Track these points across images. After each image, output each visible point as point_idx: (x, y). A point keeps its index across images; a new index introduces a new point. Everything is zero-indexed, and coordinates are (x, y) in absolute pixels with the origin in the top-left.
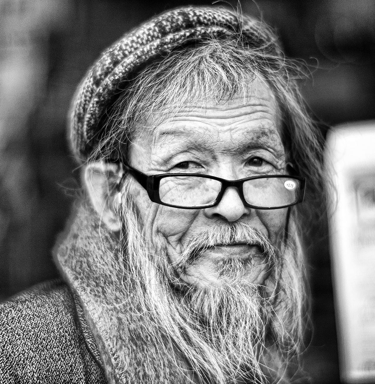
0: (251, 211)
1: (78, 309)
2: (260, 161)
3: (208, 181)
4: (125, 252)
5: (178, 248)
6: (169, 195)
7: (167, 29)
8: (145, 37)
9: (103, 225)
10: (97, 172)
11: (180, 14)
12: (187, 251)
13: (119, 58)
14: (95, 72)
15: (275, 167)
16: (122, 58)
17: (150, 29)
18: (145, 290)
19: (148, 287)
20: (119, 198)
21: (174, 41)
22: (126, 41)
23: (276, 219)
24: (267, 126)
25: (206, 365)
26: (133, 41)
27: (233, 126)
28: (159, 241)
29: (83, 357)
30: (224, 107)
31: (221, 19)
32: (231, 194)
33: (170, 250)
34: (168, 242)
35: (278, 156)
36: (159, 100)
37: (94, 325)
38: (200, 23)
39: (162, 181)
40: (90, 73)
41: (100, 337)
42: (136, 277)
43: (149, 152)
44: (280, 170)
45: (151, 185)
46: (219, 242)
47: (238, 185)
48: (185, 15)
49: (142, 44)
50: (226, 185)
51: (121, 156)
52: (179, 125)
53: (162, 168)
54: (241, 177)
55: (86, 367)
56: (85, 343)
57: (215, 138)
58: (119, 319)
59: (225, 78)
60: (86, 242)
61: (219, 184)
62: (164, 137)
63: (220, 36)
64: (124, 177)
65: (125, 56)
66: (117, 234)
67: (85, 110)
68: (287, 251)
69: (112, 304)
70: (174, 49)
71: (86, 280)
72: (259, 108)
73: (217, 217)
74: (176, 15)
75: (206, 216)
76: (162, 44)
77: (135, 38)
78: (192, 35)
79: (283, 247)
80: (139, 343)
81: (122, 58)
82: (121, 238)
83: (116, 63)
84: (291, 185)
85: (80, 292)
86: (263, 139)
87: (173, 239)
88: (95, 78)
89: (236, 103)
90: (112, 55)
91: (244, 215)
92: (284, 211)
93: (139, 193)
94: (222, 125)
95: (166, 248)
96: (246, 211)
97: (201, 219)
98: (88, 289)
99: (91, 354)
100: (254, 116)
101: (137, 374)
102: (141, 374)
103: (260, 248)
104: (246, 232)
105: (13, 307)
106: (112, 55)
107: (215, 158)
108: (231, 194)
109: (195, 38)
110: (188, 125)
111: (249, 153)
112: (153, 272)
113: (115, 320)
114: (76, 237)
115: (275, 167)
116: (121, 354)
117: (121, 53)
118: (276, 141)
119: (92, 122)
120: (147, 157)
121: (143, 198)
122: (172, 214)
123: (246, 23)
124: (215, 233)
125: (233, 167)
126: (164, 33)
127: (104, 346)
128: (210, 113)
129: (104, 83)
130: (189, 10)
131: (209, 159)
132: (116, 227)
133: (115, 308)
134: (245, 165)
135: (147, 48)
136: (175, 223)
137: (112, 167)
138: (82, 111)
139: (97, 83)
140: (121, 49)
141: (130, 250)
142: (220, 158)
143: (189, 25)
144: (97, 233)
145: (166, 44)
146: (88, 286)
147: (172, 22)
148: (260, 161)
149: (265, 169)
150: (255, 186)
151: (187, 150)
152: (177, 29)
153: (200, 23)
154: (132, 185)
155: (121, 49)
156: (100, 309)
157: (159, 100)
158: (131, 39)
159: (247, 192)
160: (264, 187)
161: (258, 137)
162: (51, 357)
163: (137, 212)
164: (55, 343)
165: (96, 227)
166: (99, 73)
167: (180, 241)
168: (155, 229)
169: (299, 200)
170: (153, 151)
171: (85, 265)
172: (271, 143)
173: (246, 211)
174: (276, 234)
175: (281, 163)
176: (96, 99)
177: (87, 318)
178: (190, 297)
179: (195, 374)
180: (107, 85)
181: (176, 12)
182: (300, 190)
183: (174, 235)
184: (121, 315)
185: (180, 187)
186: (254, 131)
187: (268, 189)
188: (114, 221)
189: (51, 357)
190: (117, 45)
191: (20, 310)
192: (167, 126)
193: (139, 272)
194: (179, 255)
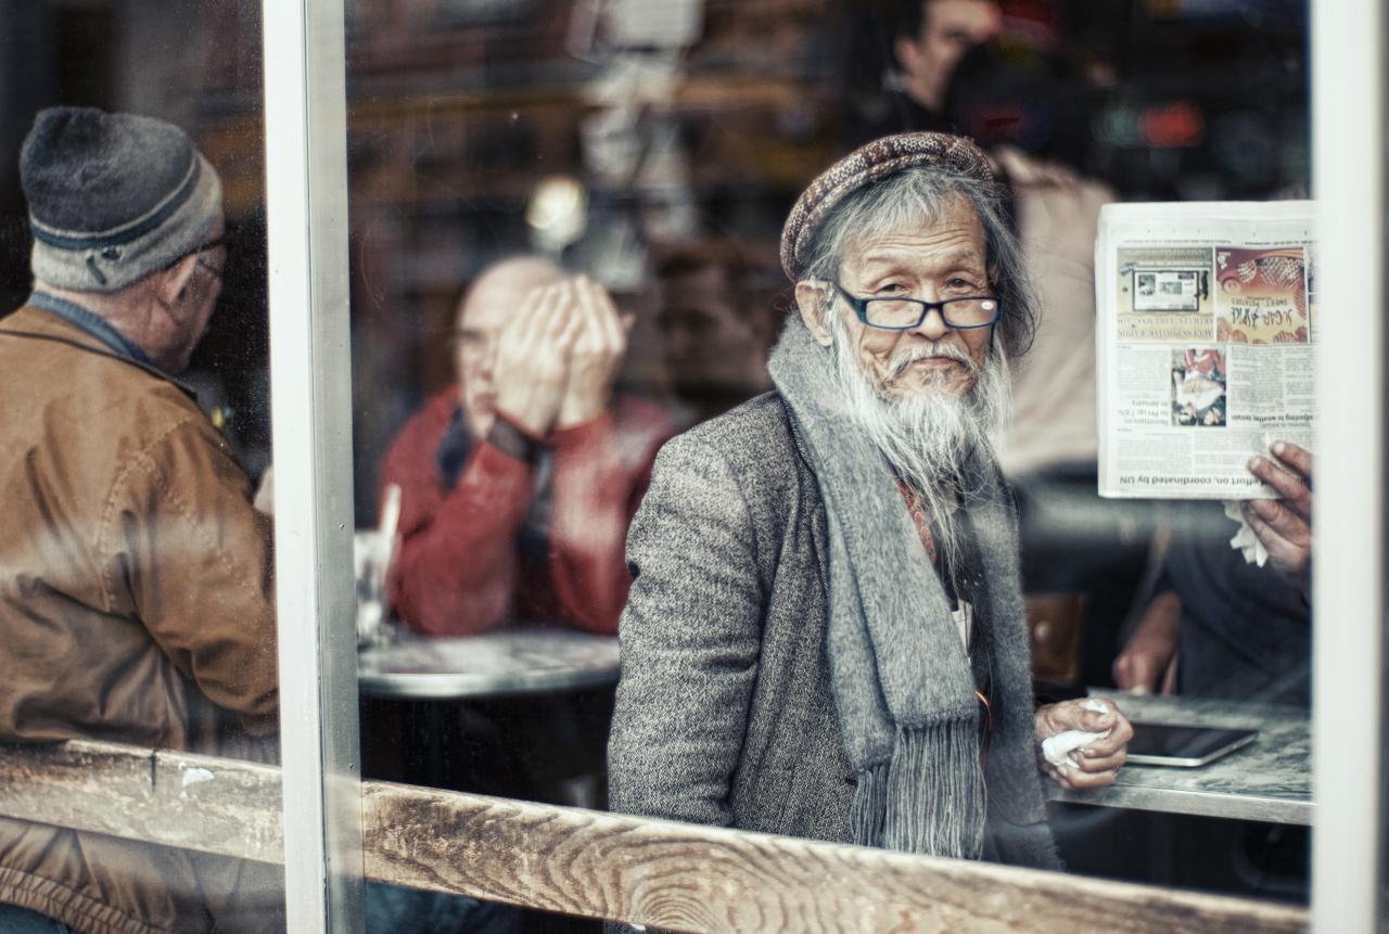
0: (950, 330)
1: (792, 421)
2: (961, 283)
3: (911, 304)
4: (836, 366)
5: (885, 363)
6: (875, 316)
7: (873, 159)
8: (853, 168)
9: (815, 340)
10: (808, 289)
11: (885, 144)
12: (894, 365)
13: (828, 187)
14: (806, 199)
15: (975, 287)
16: (832, 188)
17: (856, 161)
18: (854, 402)
19: (856, 400)
20: (831, 315)
21: (879, 171)
22: (835, 171)
23: (977, 337)
24: (966, 249)
25: (912, 472)
26: (841, 172)
27: (934, 252)
28: (868, 357)
29: (796, 464)
30: (925, 235)
31: (924, 146)
32: (933, 316)
33: (878, 365)
34: (875, 358)
35: (979, 277)
36: (866, 229)
37: (807, 435)
38: (905, 152)
39: (869, 304)
40: (801, 200)
41: (813, 446)
42: (921, 434)
43: (858, 276)
44: (979, 289)
45: (861, 307)
46: (922, 356)
47: (939, 307)
48: (890, 145)
49: (850, 174)
50: (927, 307)
51: (832, 277)
52: (885, 252)
53: (870, 291)
54: (943, 298)
55: (799, 474)
56: (799, 452)
57: (918, 264)
58: (831, 430)
59: (926, 211)
60: (798, 357)
61: (920, 307)
62: (870, 264)
63: (924, 164)
64: (834, 296)
65: (834, 186)
66: (828, 348)
67: (797, 233)
68: (992, 370)
69: (823, 416)
70: (878, 180)
71: (799, 394)
72: (960, 233)
73: (919, 335)
74: (881, 144)
75: (910, 334)
76: (868, 176)
77: (843, 169)
78: (896, 165)
79: (987, 362)
80: (848, 451)
81: (832, 188)
82: (832, 350)
83: (826, 192)
84: (988, 305)
85: (794, 405)
86: (963, 262)
87: (880, 356)
88: (806, 205)
89: (938, 230)
90: (822, 183)
91: (945, 334)
92: (990, 327)
93: (848, 313)
94: (924, 251)
95: (873, 364)
96: (947, 330)
97: (905, 338)
98: (802, 402)
99: (804, 462)
100: (955, 240)
101: (846, 478)
102: (850, 479)
103: (961, 364)
104: (949, 348)
105: (732, 419)
106: (822, 183)
107: (918, 282)
108: (933, 316)
109: (900, 167)
110: (892, 252)
111: (948, 276)
112: (862, 385)
113: (826, 431)
114: (788, 351)
115: (975, 287)
116: (832, 461)
117: (830, 182)
118: (976, 263)
119: (804, 244)
120: (857, 281)
121: (852, 317)
122: (879, 334)
123: (951, 146)
124: (918, 350)
125: (935, 290)
126: (871, 164)
127: (816, 453)
128: (913, 240)
129: (815, 211)
130: (892, 139)
131: (913, 282)
132: (828, 342)
133: (827, 420)
134: (282, 810)
135: (855, 179)
136: (883, 341)
137: (823, 285)
138: (793, 233)
139: (809, 209)
140: (830, 178)
141: (841, 365)
142: (923, 281)
143: (894, 155)
144: (809, 348)
145: (872, 175)
146: (801, 398)
147: (878, 154)
148: (961, 283)
149: (965, 289)
150: (957, 306)
151: (894, 273)
152: (882, 159)
153: (905, 152)
154: (841, 304)
155: (830, 178)
156: (813, 420)
157: (866, 229)
158: (839, 169)
159: (116, 779)
160: (964, 307)
161: (958, 260)
162: (768, 464)
163: (848, 330)
164: (772, 452)
165: (808, 342)
166: (810, 200)
167: (887, 357)
168: (862, 346)
169: (998, 318)
170: (862, 275)
171: (797, 379)
172: (970, 265)
173: (947, 330)
174: (978, 350)
175: (982, 283)
176: (807, 225)
177: (800, 429)
178: (897, 407)
179: (902, 481)
180: (817, 214)
181: (882, 141)
182: (999, 306)
183: (881, 352)
184: (831, 426)
185: (886, 309)
186: (954, 256)
187: (967, 309)
188: (825, 336)
189: (768, 464)
190: (827, 174)
191: (739, 423)
192: (874, 253)
193: (849, 385)
194: (888, 371)
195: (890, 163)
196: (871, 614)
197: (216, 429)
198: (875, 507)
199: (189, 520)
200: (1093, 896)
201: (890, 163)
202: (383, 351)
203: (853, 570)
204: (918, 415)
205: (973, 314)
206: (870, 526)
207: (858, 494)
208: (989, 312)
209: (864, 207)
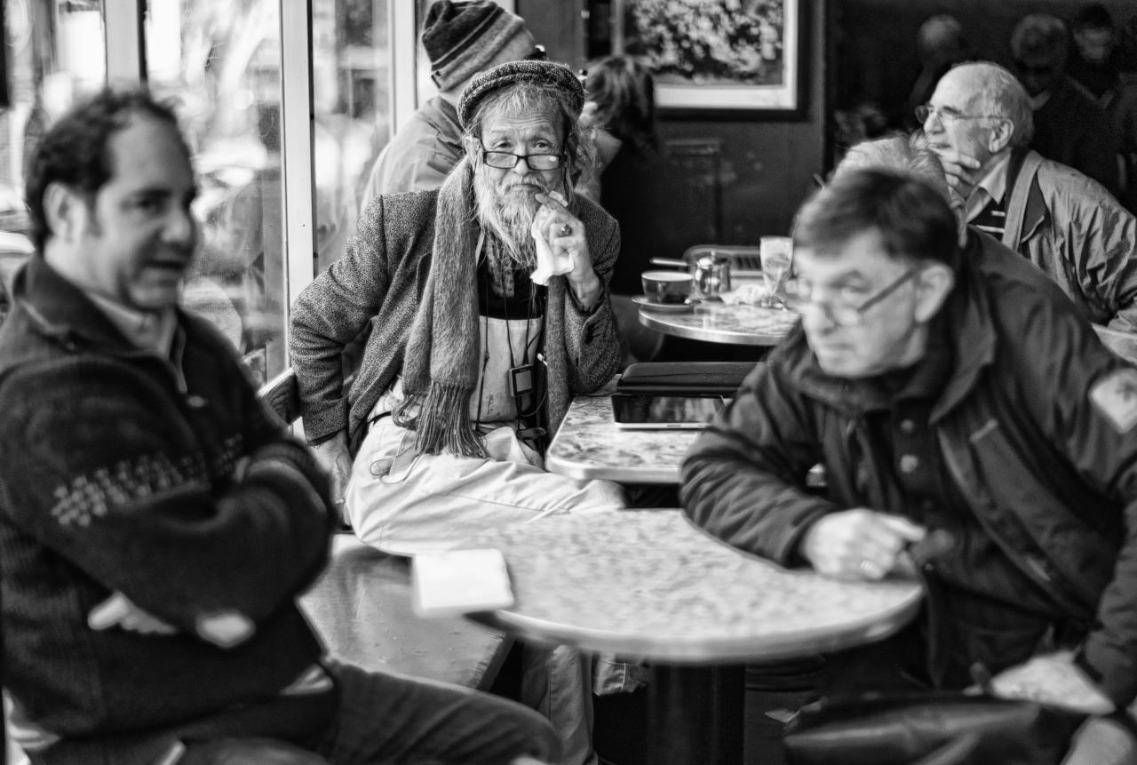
38: (519, 71)
50: (519, 158)
61: (516, 158)
63: (526, 80)
65: (479, 85)
84: (553, 159)
153: (519, 71)
195: (510, 77)
196: (435, 321)
197: (594, 695)
198: (455, 267)
199: (674, 297)
200: (471, 402)
201: (510, 77)
202: (43, 165)
203: (432, 296)
204: (514, 214)
205: (546, 161)
206: (449, 276)
207: (449, 257)
208: (555, 162)
209: (444, 119)
